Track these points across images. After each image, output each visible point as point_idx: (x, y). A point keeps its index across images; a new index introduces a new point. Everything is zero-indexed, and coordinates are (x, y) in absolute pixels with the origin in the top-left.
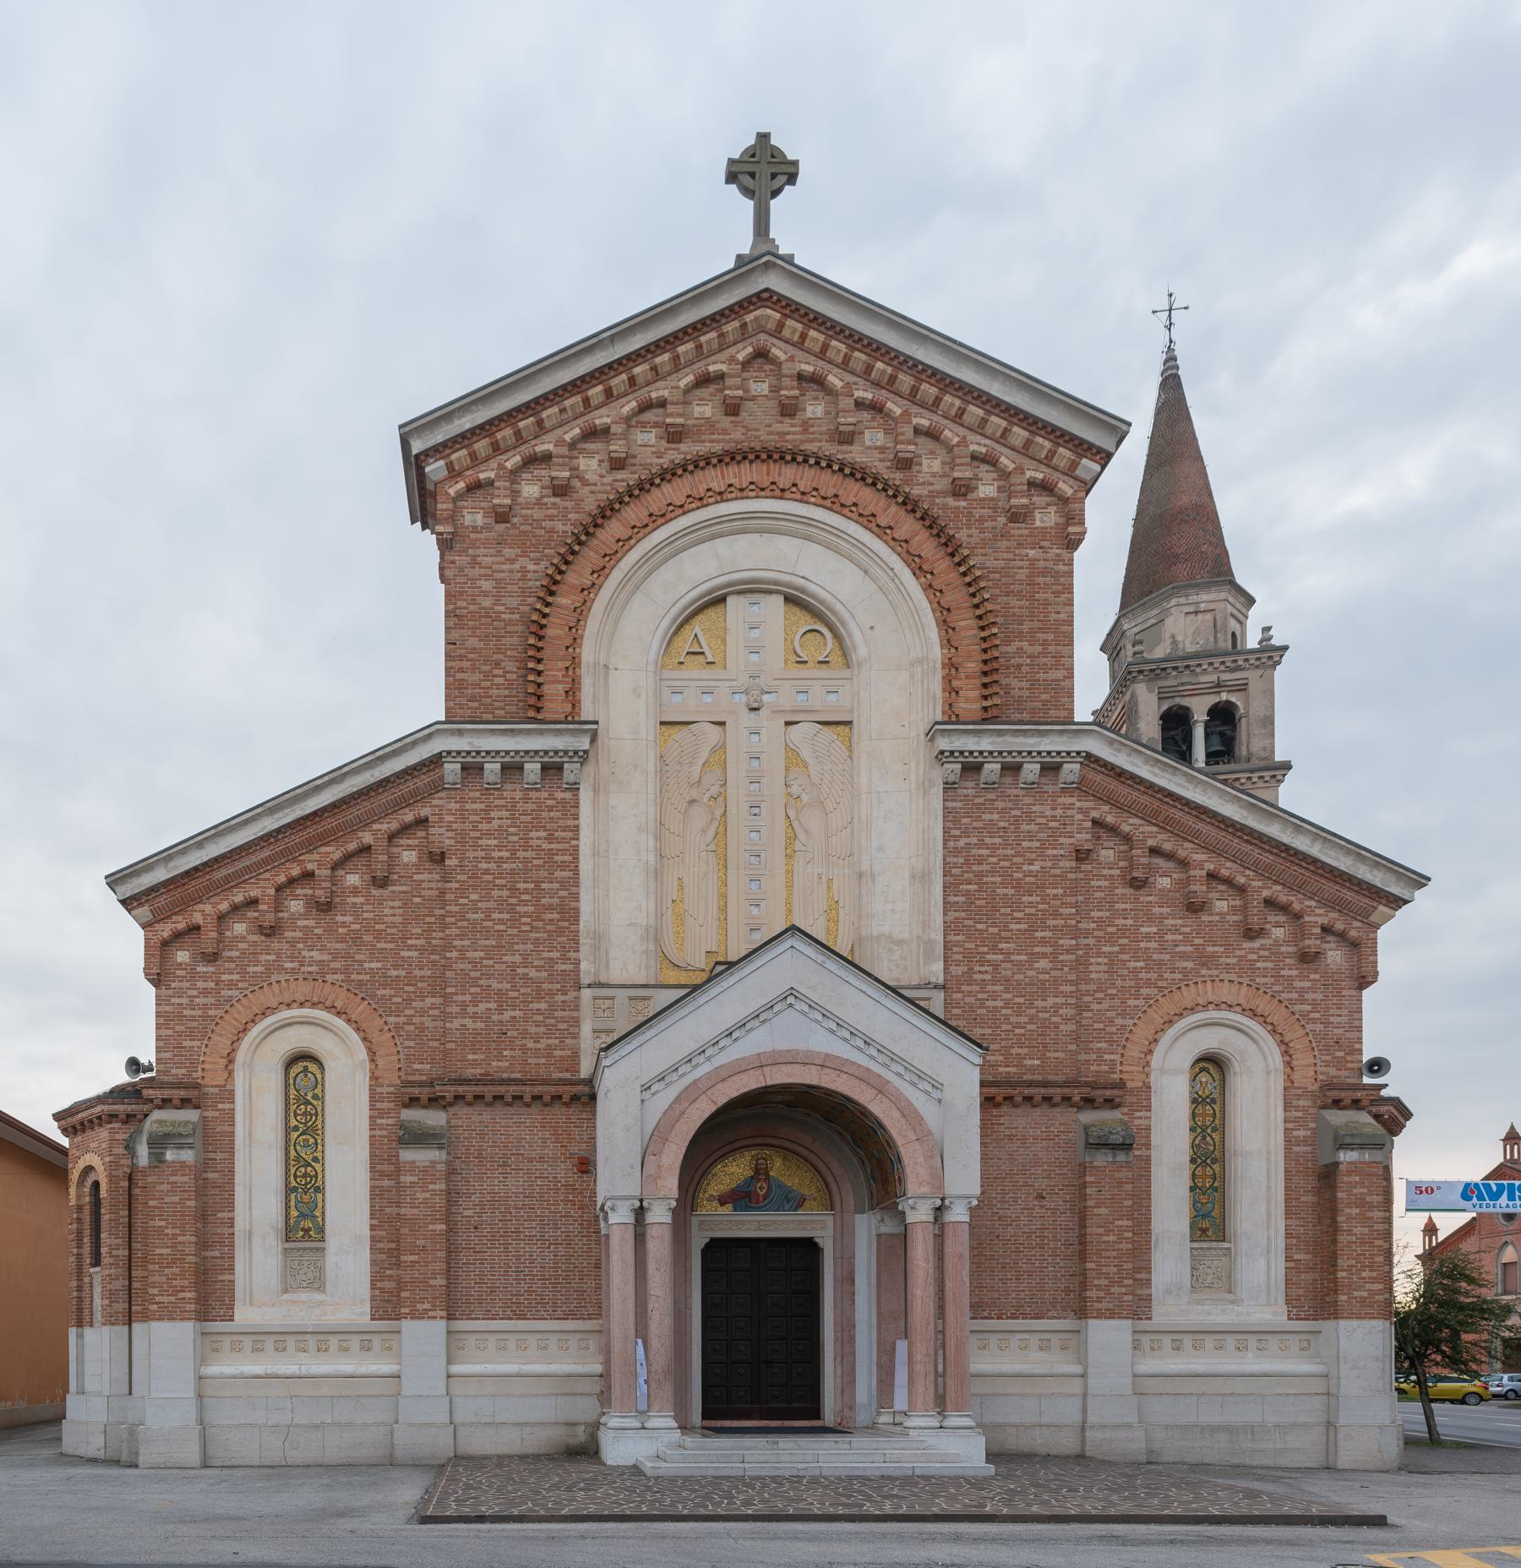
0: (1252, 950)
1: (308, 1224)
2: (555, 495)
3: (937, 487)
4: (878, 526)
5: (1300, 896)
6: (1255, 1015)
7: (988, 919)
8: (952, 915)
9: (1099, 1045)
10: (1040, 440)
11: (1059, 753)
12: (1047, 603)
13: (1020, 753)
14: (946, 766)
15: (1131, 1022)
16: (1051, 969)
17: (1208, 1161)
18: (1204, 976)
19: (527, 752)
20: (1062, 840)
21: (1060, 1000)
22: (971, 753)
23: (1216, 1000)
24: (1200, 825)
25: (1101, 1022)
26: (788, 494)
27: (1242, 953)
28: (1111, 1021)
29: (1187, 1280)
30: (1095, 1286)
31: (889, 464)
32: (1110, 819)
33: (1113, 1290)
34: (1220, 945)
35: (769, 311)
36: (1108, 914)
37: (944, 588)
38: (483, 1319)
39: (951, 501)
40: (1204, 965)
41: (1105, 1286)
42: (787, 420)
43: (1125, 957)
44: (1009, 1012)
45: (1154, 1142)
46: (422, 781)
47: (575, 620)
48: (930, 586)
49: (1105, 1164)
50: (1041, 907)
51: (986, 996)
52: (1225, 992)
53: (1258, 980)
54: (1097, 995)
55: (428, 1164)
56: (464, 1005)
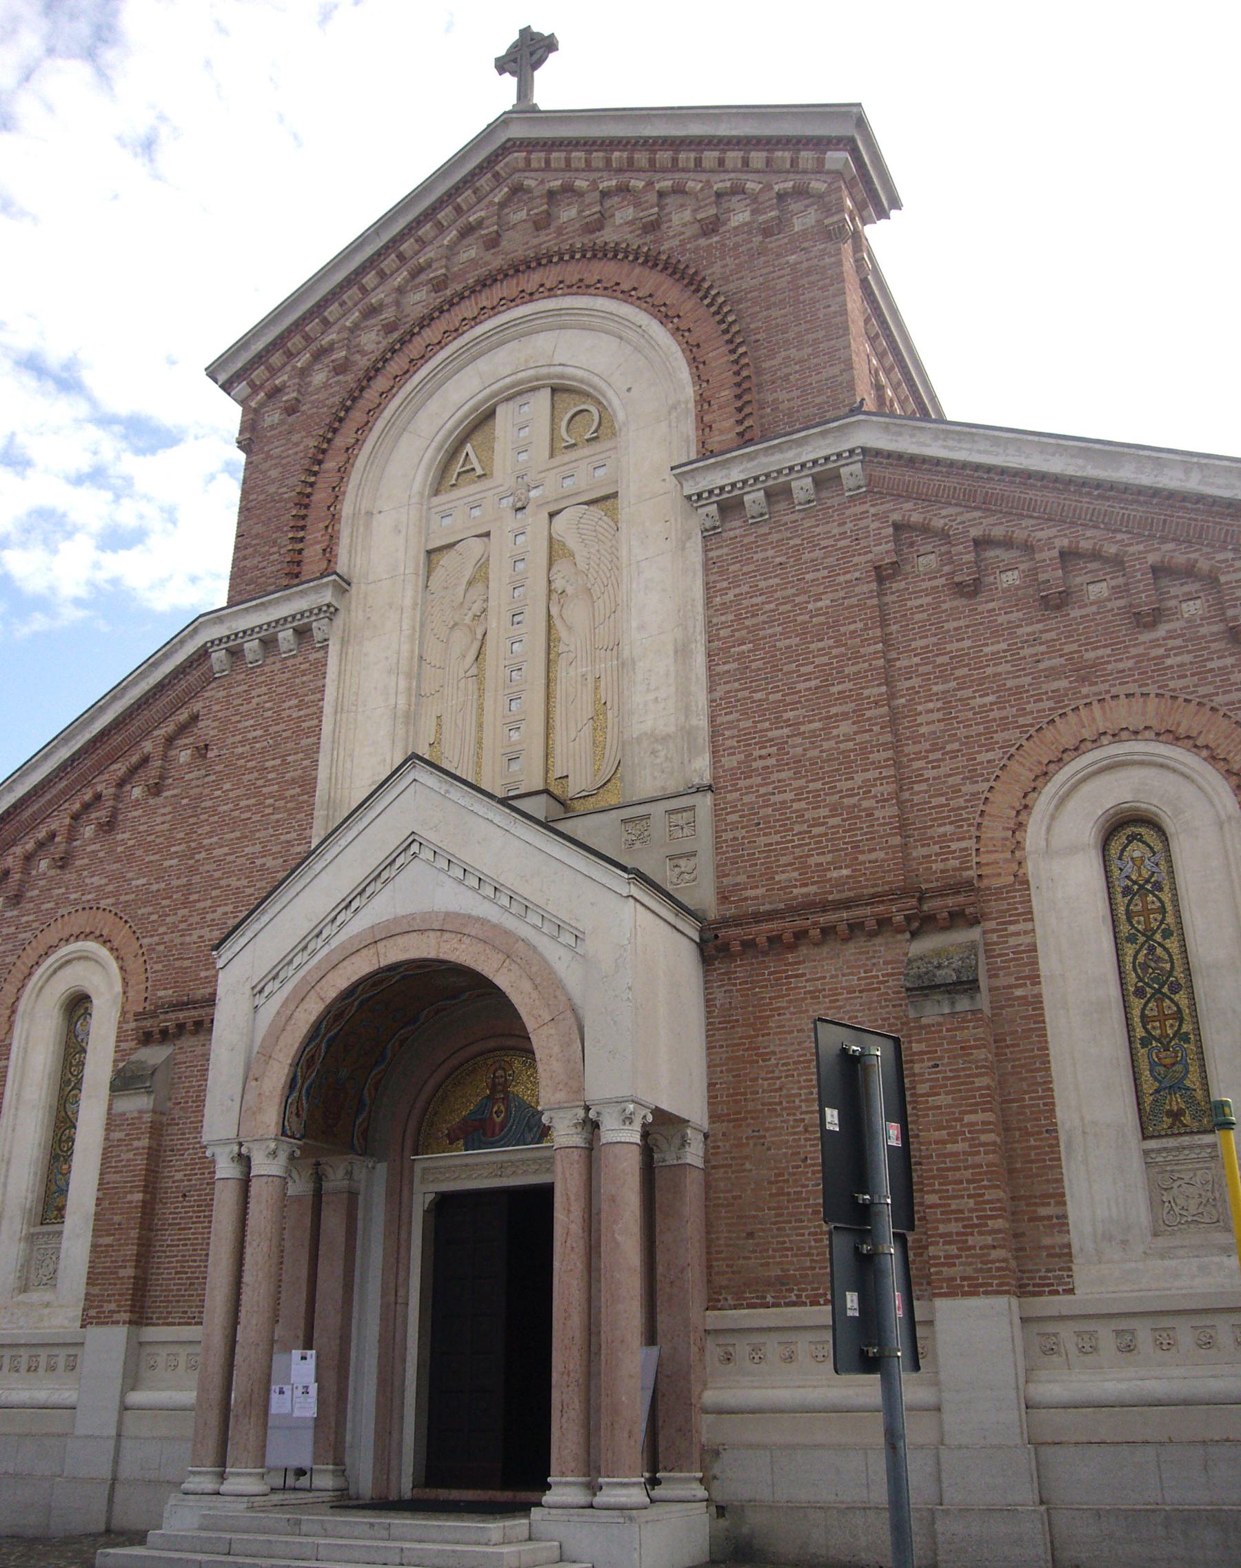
0: (1155, 644)
1: (1176, 1103)
2: (337, 374)
3: (688, 234)
4: (622, 292)
5: (1205, 550)
6: (1178, 739)
7: (768, 684)
8: (720, 692)
9: (942, 830)
10: (779, 154)
11: (827, 459)
12: (814, 301)
13: (779, 472)
14: (700, 511)
15: (986, 786)
16: (855, 733)
17: (1165, 990)
18: (1087, 696)
19: (277, 622)
20: (856, 560)
21: (871, 775)
22: (722, 489)
23: (1111, 727)
24: (1031, 494)
25: (941, 795)
26: (537, 296)
27: (1141, 650)
28: (956, 790)
29: (1141, 1215)
30: (941, 1236)
31: (639, 232)
32: (916, 518)
33: (971, 1241)
34: (1105, 646)
35: (516, 155)
36: (935, 640)
37: (691, 325)
38: (180, 1324)
39: (703, 242)
40: (1083, 680)
41: (958, 1234)
42: (543, 232)
43: (968, 693)
44: (803, 805)
45: (1044, 968)
46: (193, 677)
47: (337, 479)
48: (678, 329)
49: (940, 1019)
50: (835, 652)
51: (770, 789)
52: (1123, 714)
53: (1172, 684)
54: (932, 757)
55: (136, 1115)
56: (204, 912)
